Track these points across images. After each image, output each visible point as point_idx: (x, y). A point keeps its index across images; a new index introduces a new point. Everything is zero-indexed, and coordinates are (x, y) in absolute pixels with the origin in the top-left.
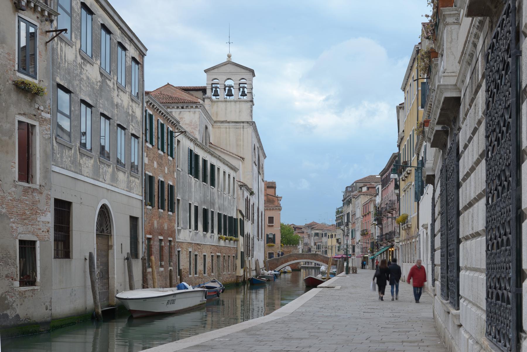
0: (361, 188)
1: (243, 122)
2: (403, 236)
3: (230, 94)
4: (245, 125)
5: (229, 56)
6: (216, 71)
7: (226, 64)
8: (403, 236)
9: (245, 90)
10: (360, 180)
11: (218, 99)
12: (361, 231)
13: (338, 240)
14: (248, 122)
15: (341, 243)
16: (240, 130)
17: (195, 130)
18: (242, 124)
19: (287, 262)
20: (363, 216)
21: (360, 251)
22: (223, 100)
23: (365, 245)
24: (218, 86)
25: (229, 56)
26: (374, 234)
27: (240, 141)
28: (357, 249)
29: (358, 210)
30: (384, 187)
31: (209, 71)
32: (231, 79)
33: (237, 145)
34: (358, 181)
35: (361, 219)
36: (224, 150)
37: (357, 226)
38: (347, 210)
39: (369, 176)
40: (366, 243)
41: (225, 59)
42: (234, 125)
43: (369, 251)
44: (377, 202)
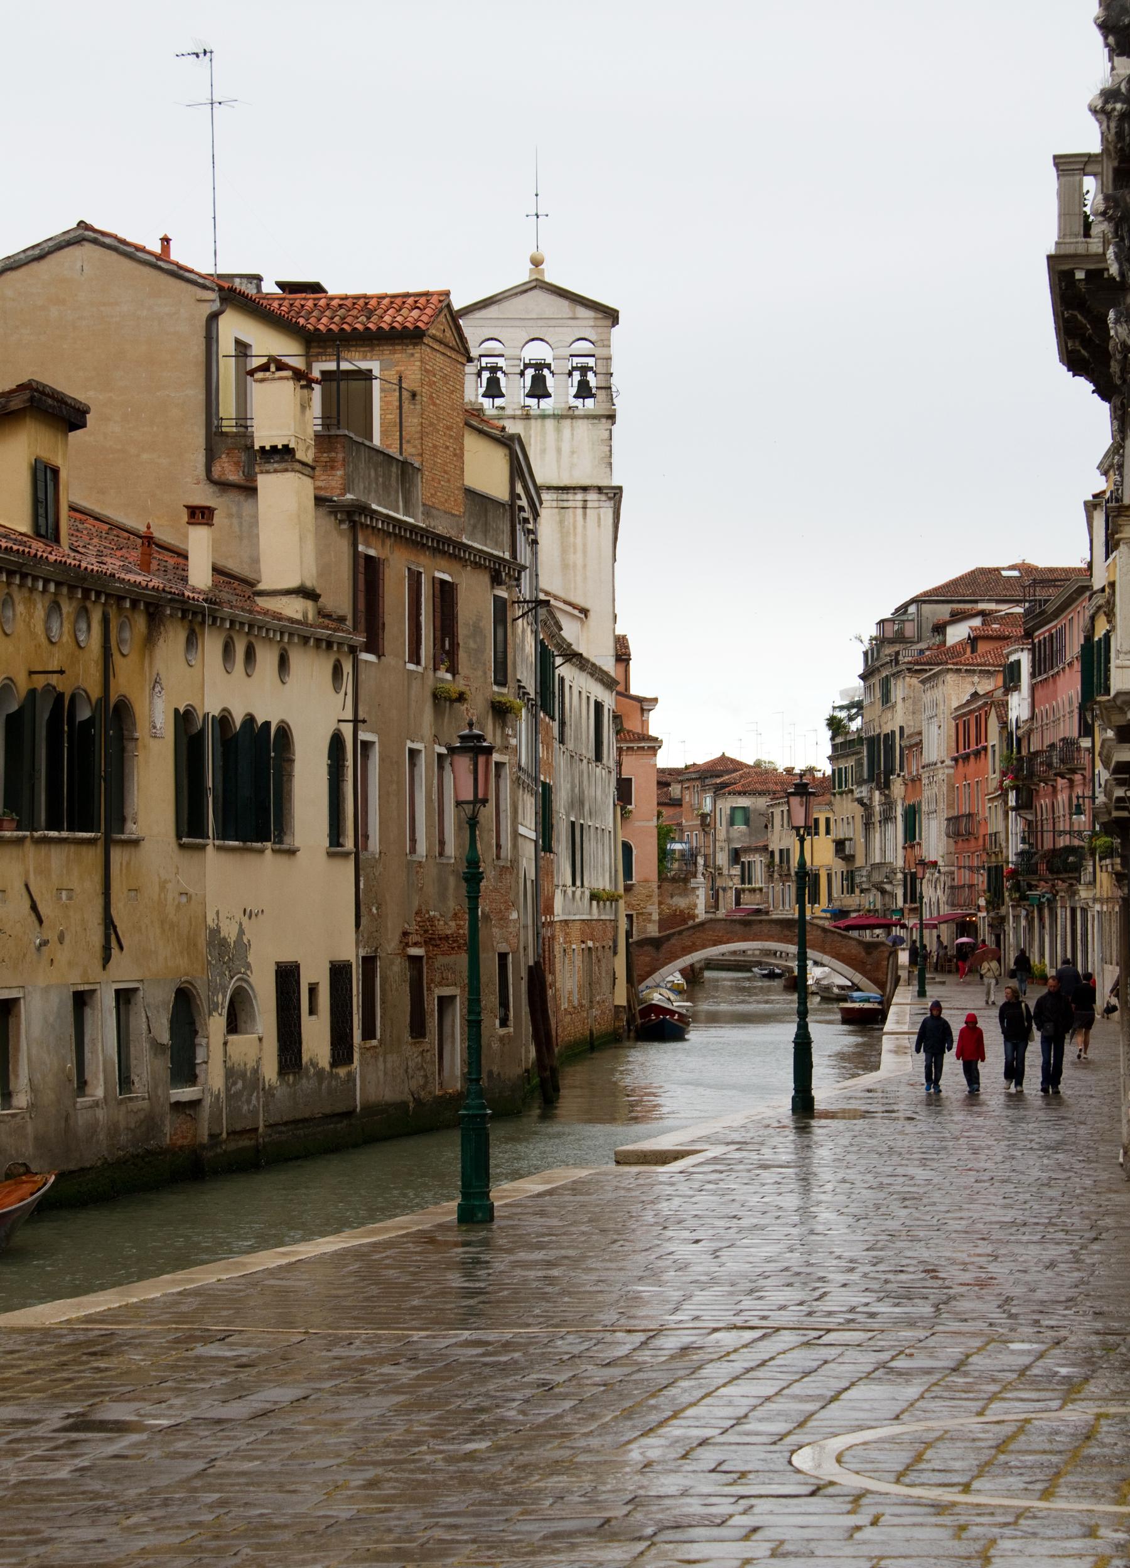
0: (940, 629)
1: (585, 489)
2: (1105, 888)
3: (539, 390)
4: (592, 496)
5: (537, 263)
6: (492, 311)
7: (525, 291)
8: (1105, 888)
9: (590, 376)
10: (936, 591)
11: (503, 408)
12: (948, 819)
13: (840, 845)
15: (853, 856)
16: (575, 515)
18: (580, 496)
19: (690, 952)
20: (956, 760)
21: (943, 899)
22: (519, 412)
23: (965, 877)
24: (501, 362)
25: (537, 263)
26: (1002, 836)
27: (575, 553)
28: (931, 891)
29: (934, 729)
30: (1040, 674)
32: (542, 340)
33: (565, 566)
34: (925, 594)
35: (946, 771)
37: (927, 793)
38: (884, 719)
39: (973, 572)
40: (971, 868)
41: (522, 274)
43: (982, 902)
44: (1013, 715)
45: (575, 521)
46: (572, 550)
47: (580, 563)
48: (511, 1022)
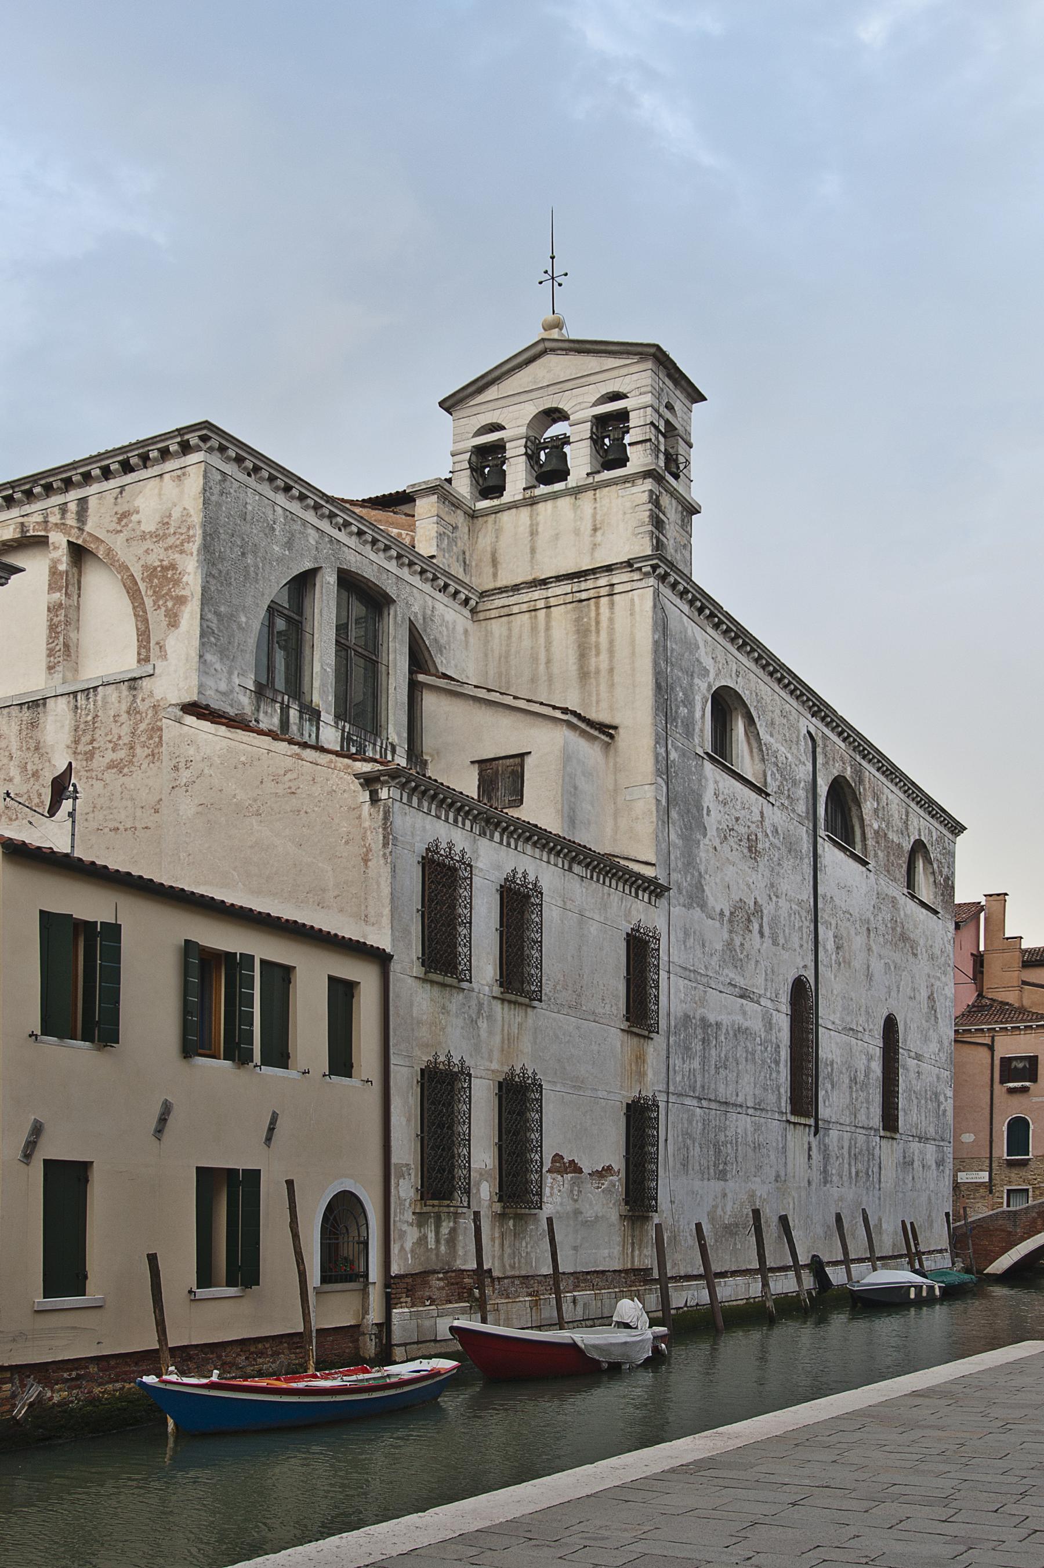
1: (609, 569)
14: (629, 564)
17: (182, 552)
27: (598, 655)
31: (461, 401)
33: (584, 675)
36: (489, 690)
42: (568, 589)
45: (598, 614)
46: (593, 652)
47: (604, 666)
48: (1002, 1130)
